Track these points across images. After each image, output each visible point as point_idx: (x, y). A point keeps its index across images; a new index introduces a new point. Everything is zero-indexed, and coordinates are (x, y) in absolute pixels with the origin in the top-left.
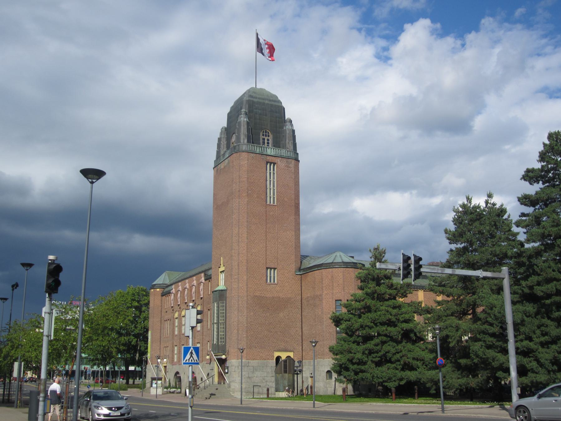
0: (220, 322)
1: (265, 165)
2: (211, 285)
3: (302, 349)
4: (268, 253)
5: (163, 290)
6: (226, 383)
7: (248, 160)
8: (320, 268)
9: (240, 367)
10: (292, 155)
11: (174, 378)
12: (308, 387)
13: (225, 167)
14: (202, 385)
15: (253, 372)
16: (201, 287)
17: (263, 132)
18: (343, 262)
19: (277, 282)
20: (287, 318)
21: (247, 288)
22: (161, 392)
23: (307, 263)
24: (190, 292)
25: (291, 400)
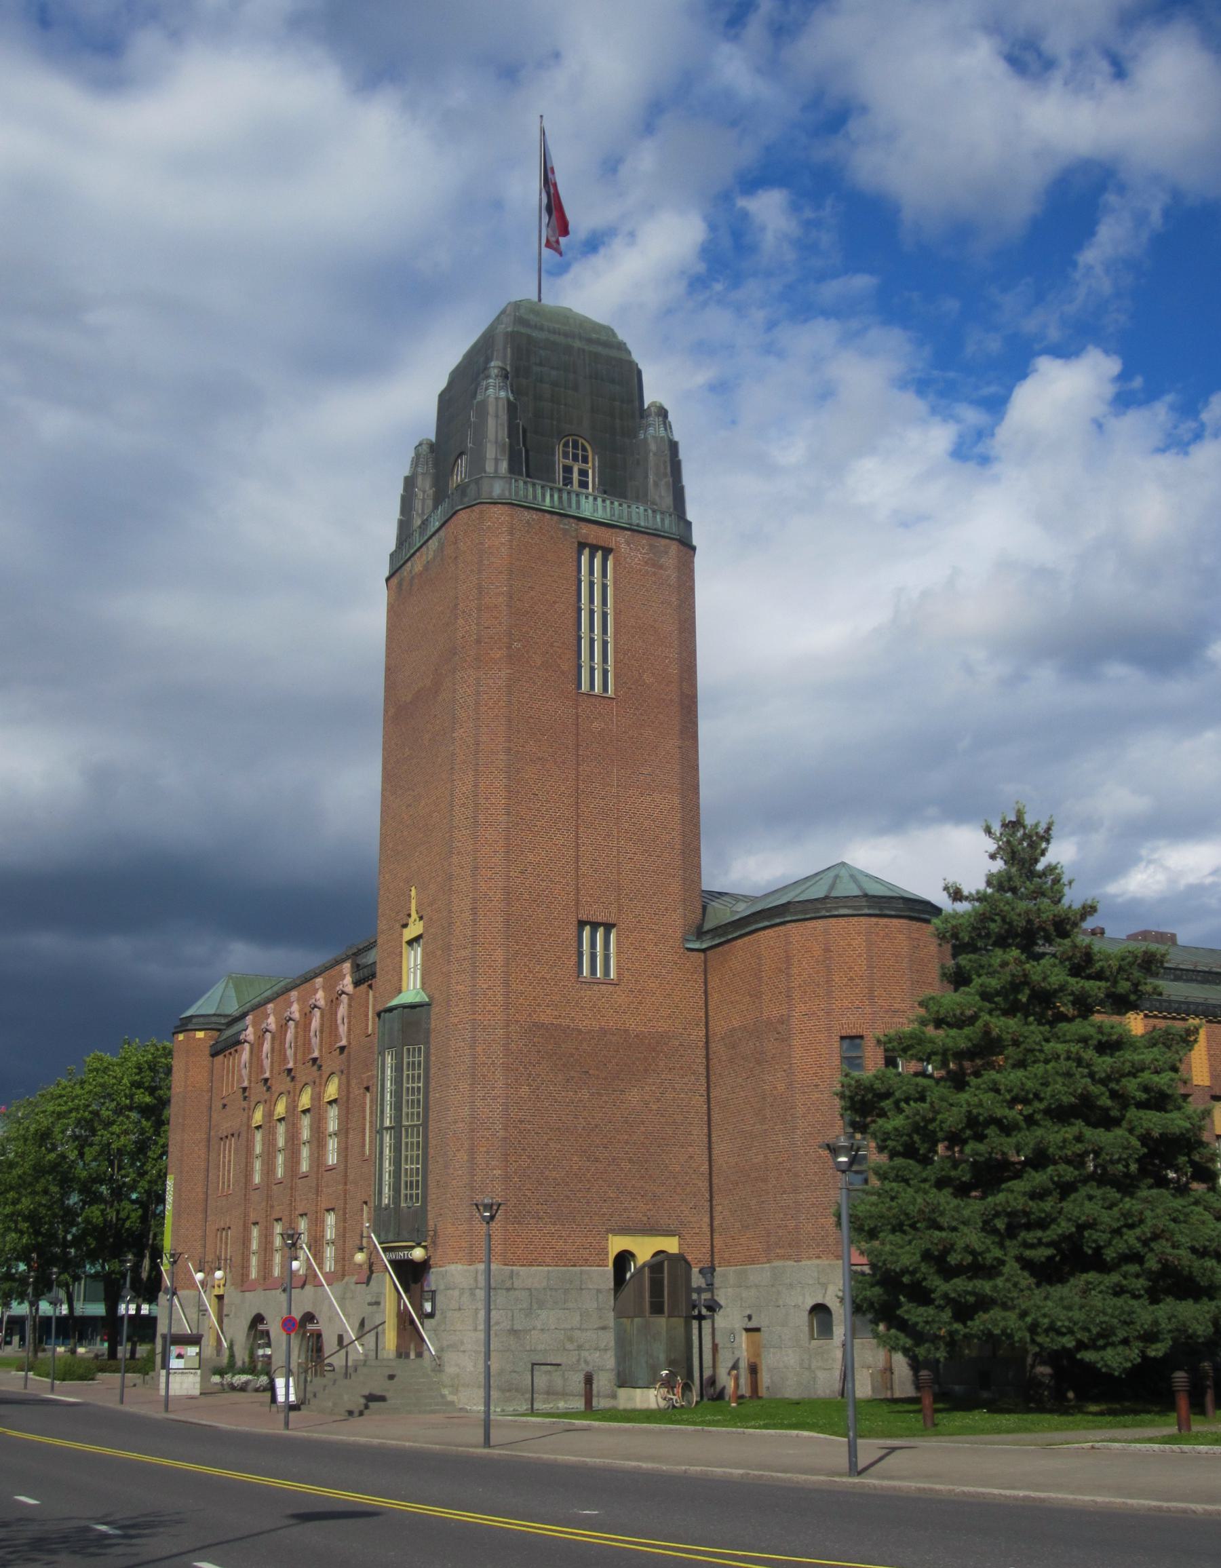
0: (405, 1123)
1: (575, 556)
2: (375, 997)
3: (711, 1225)
4: (583, 869)
5: (216, 1034)
6: (426, 1354)
7: (511, 534)
8: (778, 921)
9: (481, 1294)
10: (668, 524)
11: (248, 1335)
12: (735, 1366)
13: (426, 568)
14: (338, 1361)
15: (529, 1312)
16: (342, 1010)
17: (566, 445)
18: (866, 895)
19: (619, 974)
20: (655, 1107)
21: (507, 995)
22: (198, 1386)
23: (721, 914)
24: (305, 1031)
25: (694, 1424)
